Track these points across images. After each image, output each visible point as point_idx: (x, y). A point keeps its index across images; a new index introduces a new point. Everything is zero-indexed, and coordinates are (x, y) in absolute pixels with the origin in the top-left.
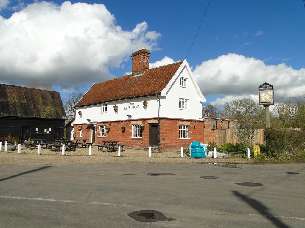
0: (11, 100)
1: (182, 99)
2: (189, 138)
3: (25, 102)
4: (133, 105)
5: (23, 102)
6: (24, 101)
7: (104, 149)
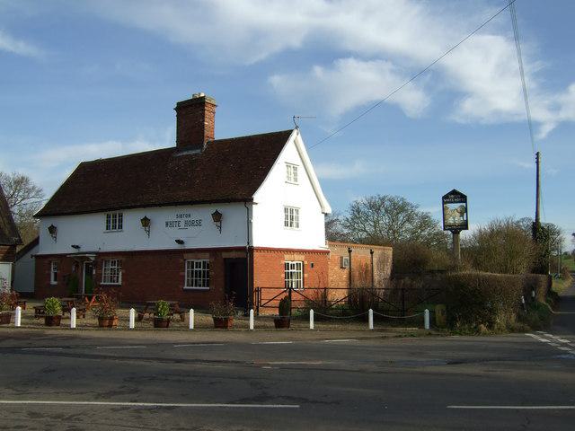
2: (120, 283)
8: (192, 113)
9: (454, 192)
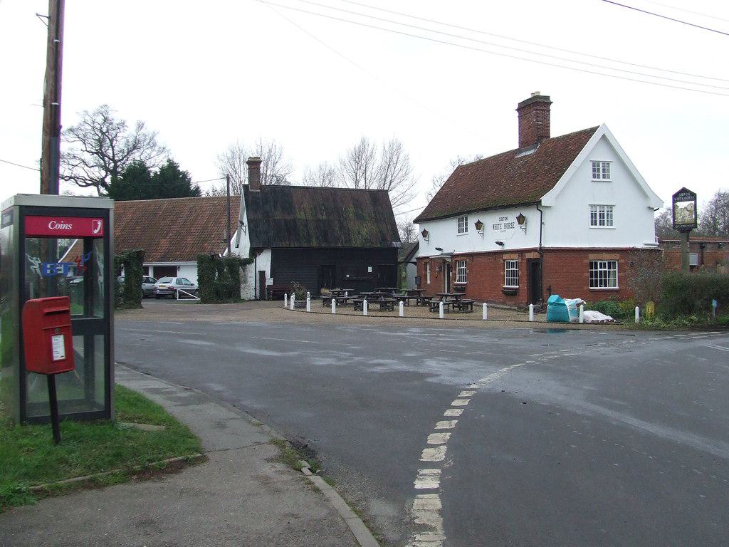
0: (300, 215)
1: (606, 207)
2: (617, 287)
3: (324, 217)
5: (320, 217)
8: (534, 110)
9: (684, 190)
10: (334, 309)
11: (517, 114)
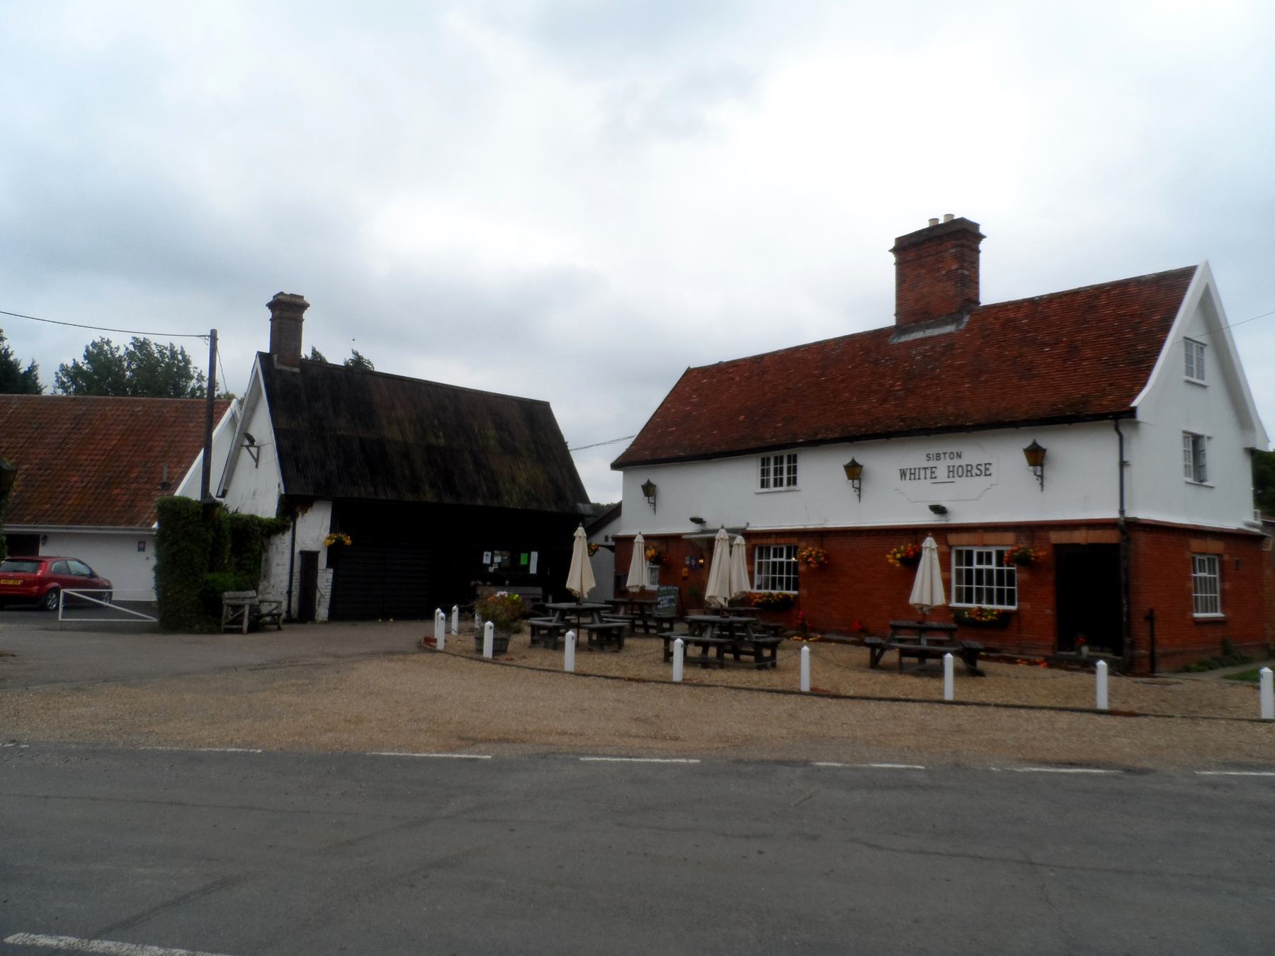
2: (1219, 614)
3: (442, 442)
4: (951, 463)
5: (433, 441)
6: (437, 436)
7: (891, 657)
10: (569, 657)
11: (892, 259)
